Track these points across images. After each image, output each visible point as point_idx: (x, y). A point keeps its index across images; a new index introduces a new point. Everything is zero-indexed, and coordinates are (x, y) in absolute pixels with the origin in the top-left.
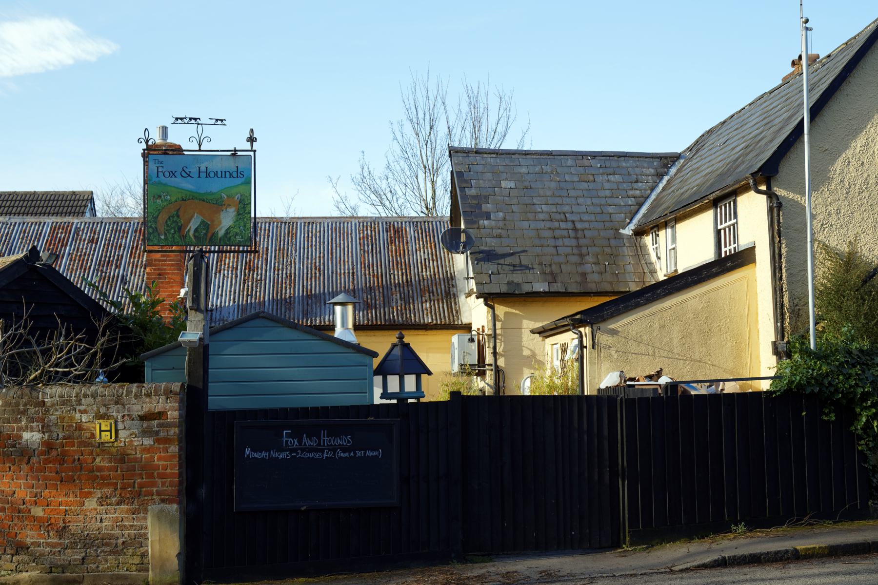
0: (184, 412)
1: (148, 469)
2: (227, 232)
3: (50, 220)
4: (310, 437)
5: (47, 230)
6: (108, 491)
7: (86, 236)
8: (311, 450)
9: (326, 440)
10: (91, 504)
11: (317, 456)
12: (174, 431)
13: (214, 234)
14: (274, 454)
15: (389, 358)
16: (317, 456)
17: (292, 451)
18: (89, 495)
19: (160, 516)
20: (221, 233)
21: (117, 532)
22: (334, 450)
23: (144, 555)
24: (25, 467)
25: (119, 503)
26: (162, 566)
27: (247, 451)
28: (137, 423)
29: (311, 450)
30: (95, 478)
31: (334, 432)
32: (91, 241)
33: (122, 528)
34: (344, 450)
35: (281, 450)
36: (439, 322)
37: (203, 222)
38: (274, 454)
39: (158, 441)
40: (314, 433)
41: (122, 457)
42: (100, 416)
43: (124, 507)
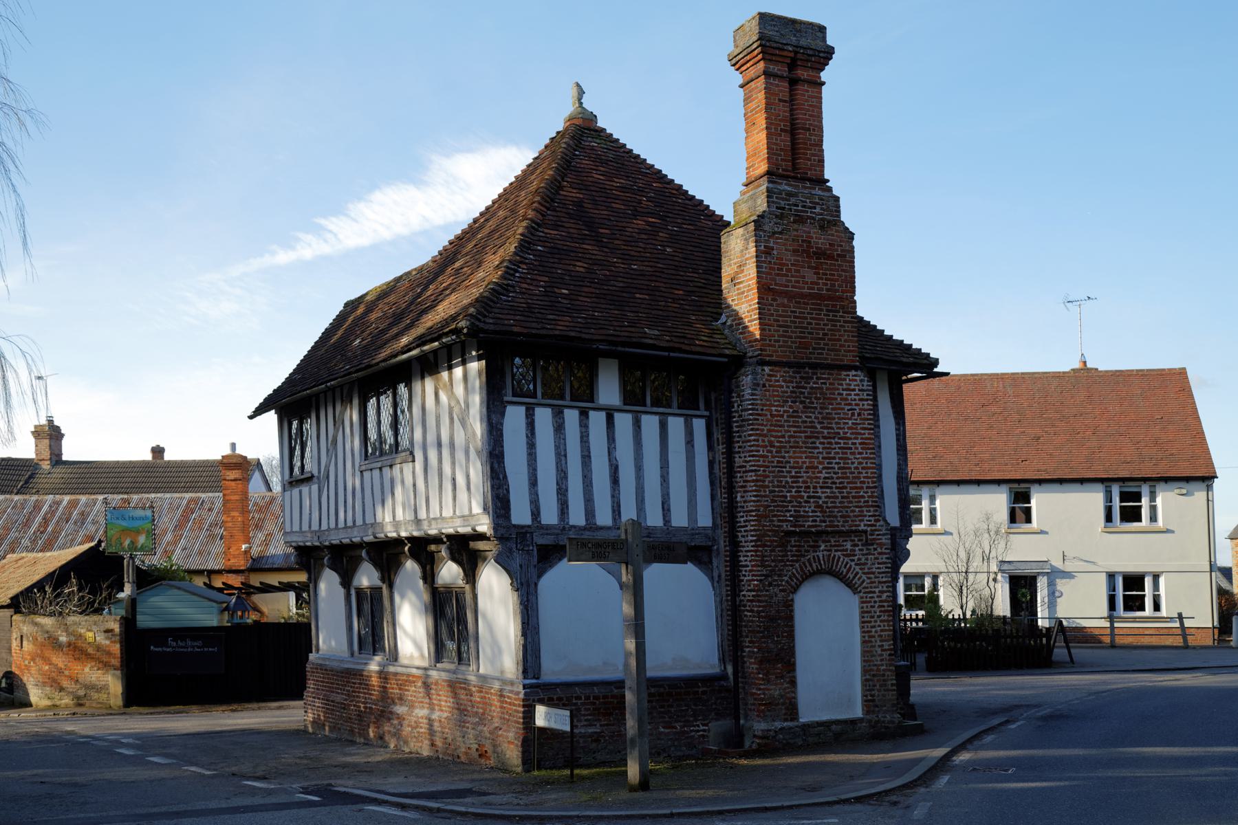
0: (123, 629)
1: (109, 653)
2: (142, 546)
3: (188, 496)
4: (181, 641)
5: (185, 502)
6: (93, 664)
7: (206, 506)
8: (182, 647)
9: (189, 643)
10: (87, 670)
11: (185, 650)
12: (118, 638)
13: (136, 547)
14: (165, 649)
15: (483, 553)
16: (185, 650)
17: (173, 647)
18: (85, 666)
19: (114, 675)
20: (139, 546)
21: (98, 683)
22: (193, 647)
23: (109, 694)
24: (61, 653)
25: (98, 670)
26: (116, 696)
27: (152, 647)
28: (103, 634)
29: (182, 647)
30: (89, 657)
31: (194, 639)
32: (209, 510)
33: (99, 681)
34: (198, 647)
35: (168, 647)
36: (577, 517)
37: (131, 541)
38: (165, 649)
39: (112, 642)
40: (183, 640)
41: (99, 648)
42: (90, 631)
43: (99, 672)
